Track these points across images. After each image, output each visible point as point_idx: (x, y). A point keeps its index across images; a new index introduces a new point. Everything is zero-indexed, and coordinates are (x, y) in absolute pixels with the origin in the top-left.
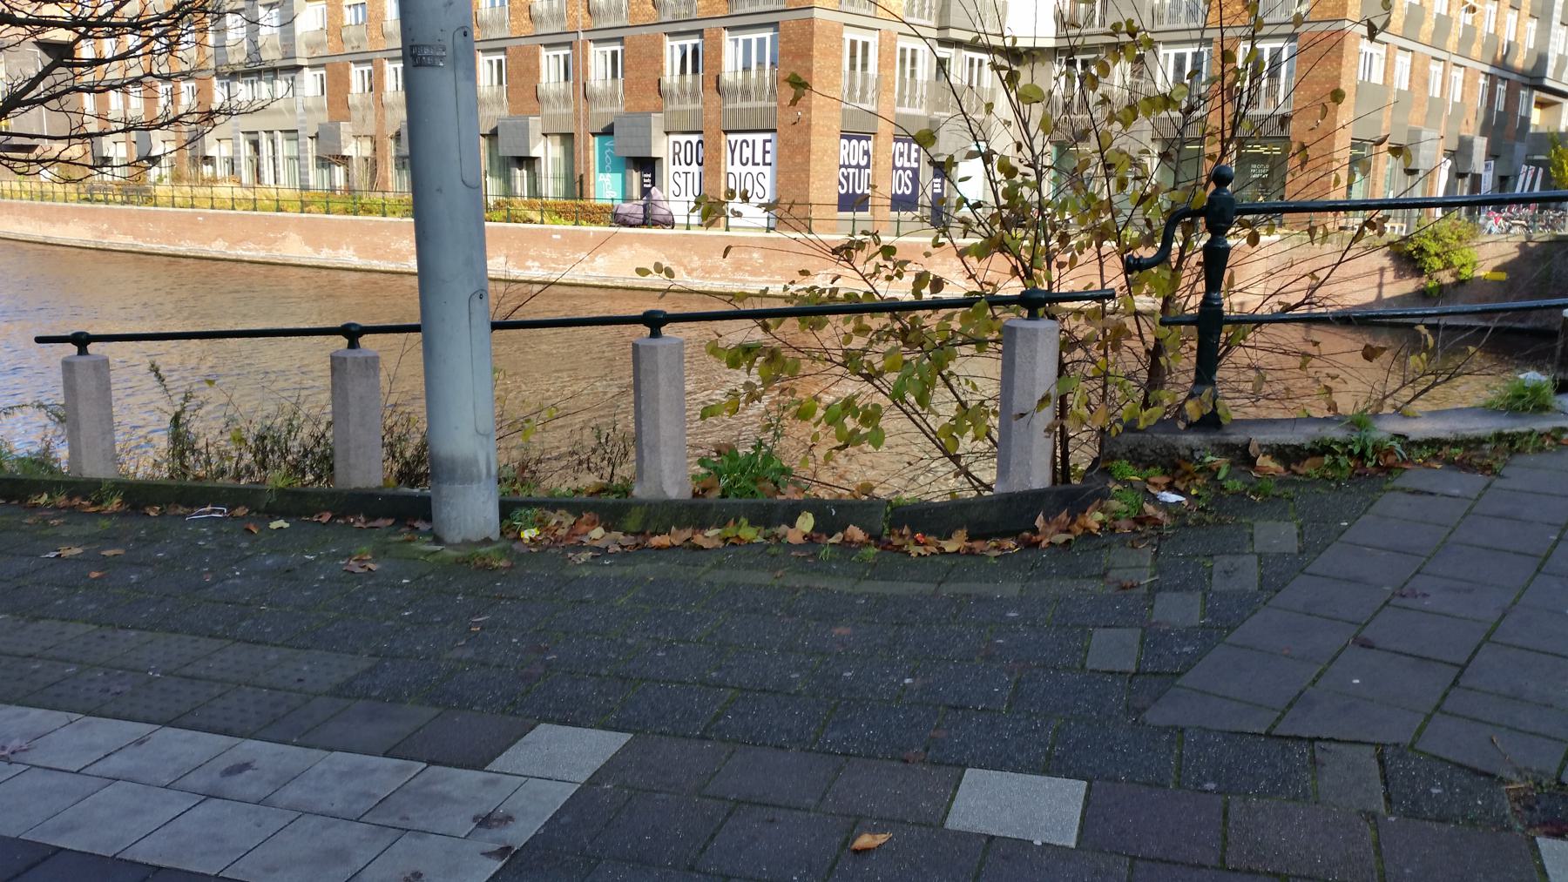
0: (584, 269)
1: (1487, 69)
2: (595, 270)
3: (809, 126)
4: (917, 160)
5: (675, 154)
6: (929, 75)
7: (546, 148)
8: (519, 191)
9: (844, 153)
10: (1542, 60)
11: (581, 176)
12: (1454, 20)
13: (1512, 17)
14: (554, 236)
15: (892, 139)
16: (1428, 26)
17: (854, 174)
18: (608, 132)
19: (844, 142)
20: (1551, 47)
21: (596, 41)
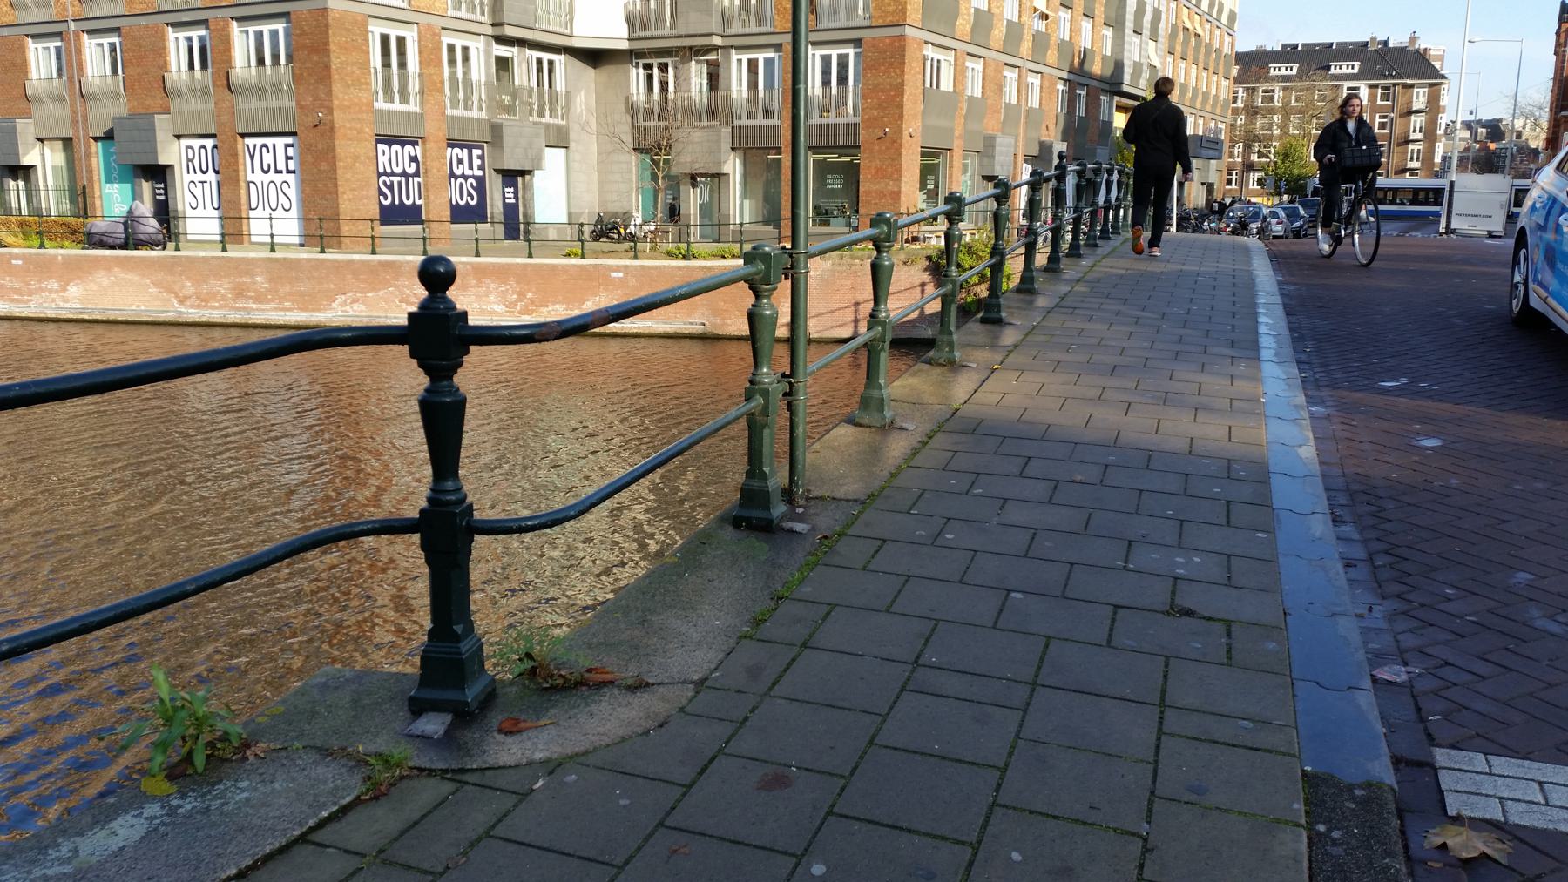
0: (54, 300)
1: (1065, 75)
2: (66, 301)
3: (332, 129)
4: (481, 167)
5: (189, 160)
6: (487, 75)
7: (43, 155)
8: (14, 204)
9: (383, 160)
10: (1119, 66)
11: (84, 187)
12: (1026, 27)
13: (1086, 25)
14: (14, 262)
15: (445, 145)
16: (998, 33)
17: (400, 183)
18: (109, 136)
19: (381, 147)
20: (1126, 54)
21: (91, 32)
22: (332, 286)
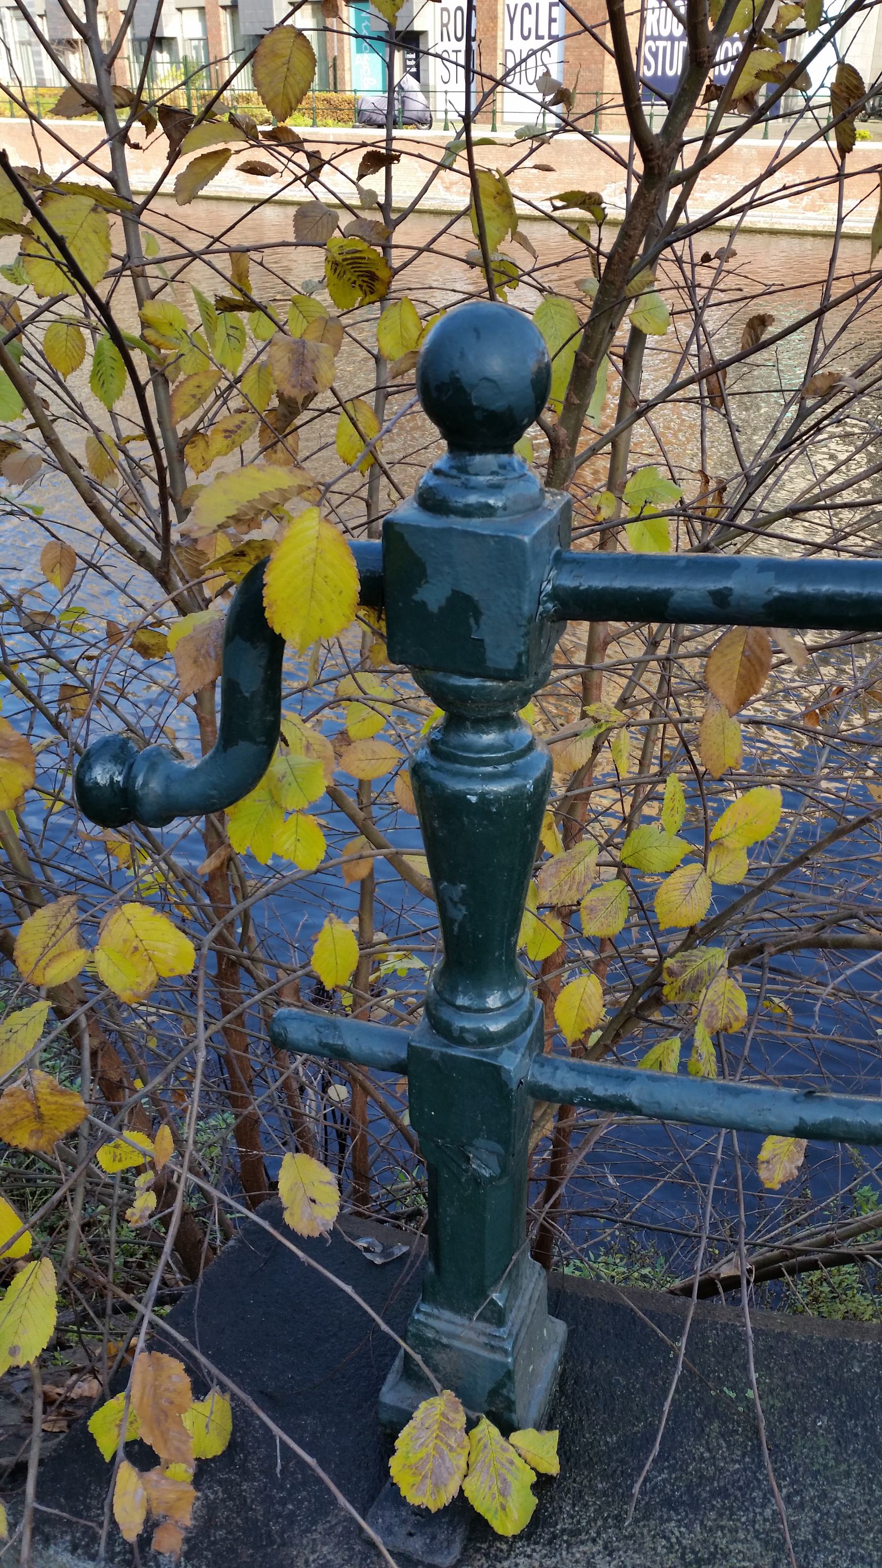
11: (335, 59)
17: (665, 49)
22: (602, 173)
